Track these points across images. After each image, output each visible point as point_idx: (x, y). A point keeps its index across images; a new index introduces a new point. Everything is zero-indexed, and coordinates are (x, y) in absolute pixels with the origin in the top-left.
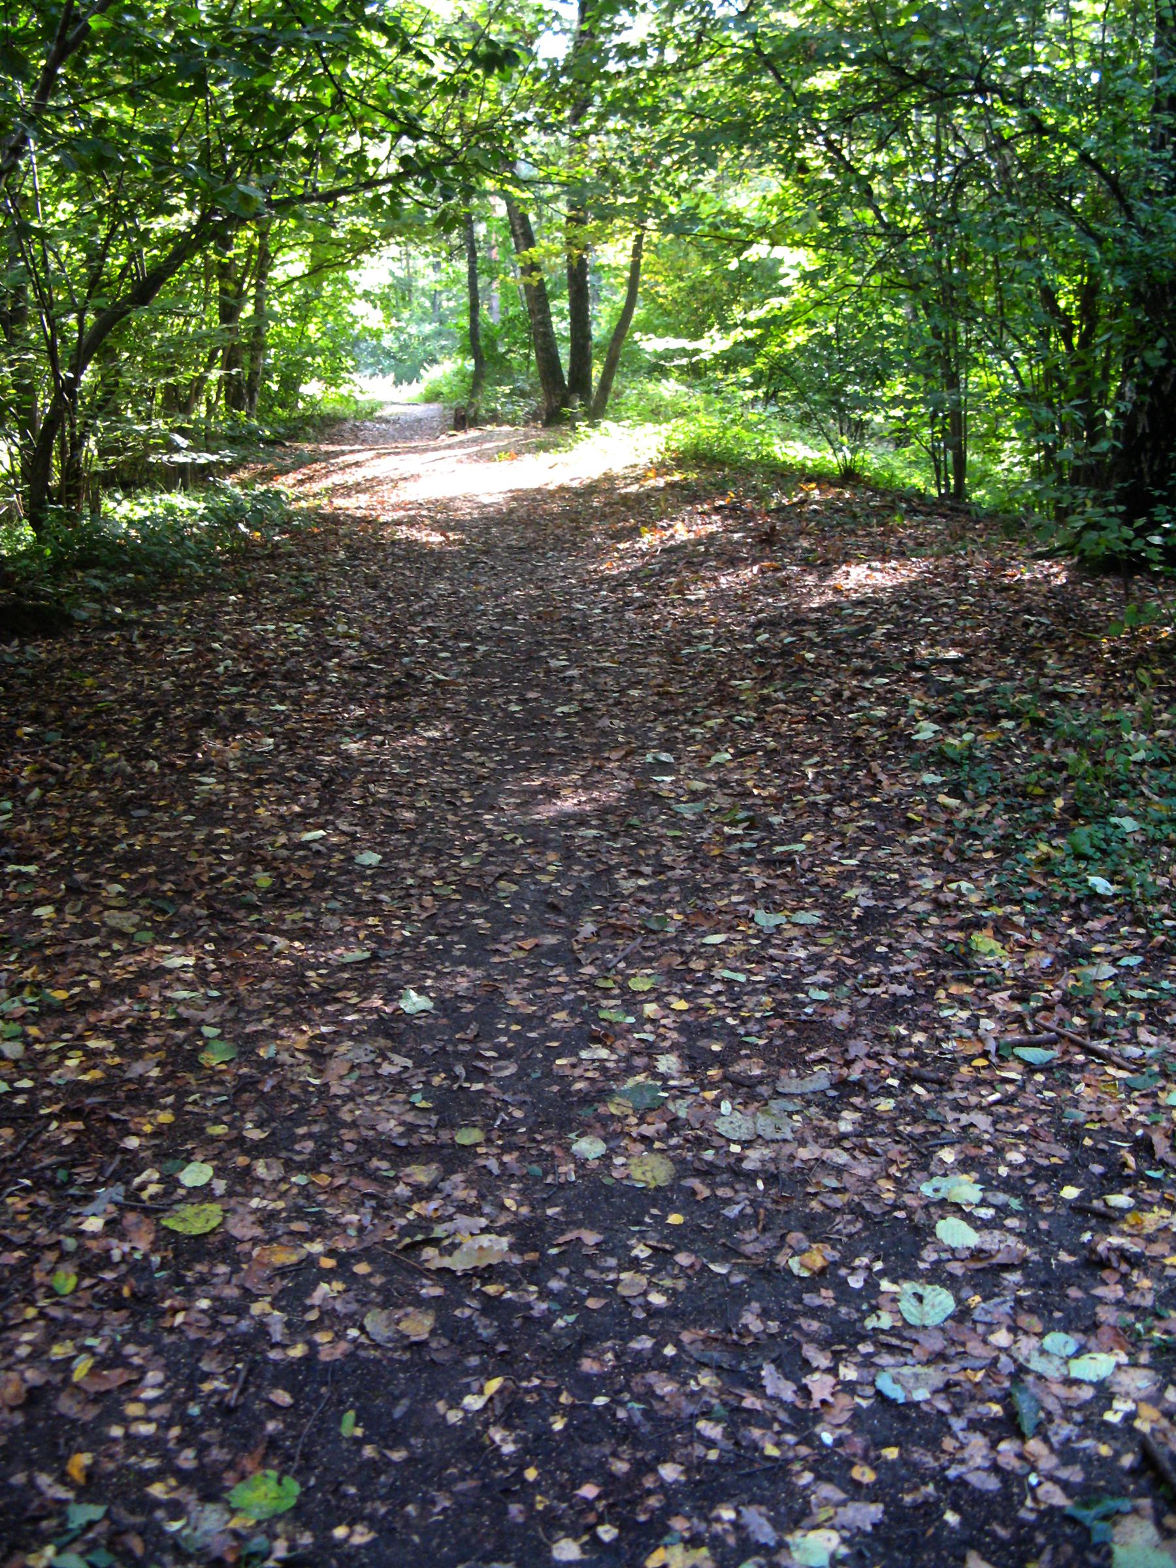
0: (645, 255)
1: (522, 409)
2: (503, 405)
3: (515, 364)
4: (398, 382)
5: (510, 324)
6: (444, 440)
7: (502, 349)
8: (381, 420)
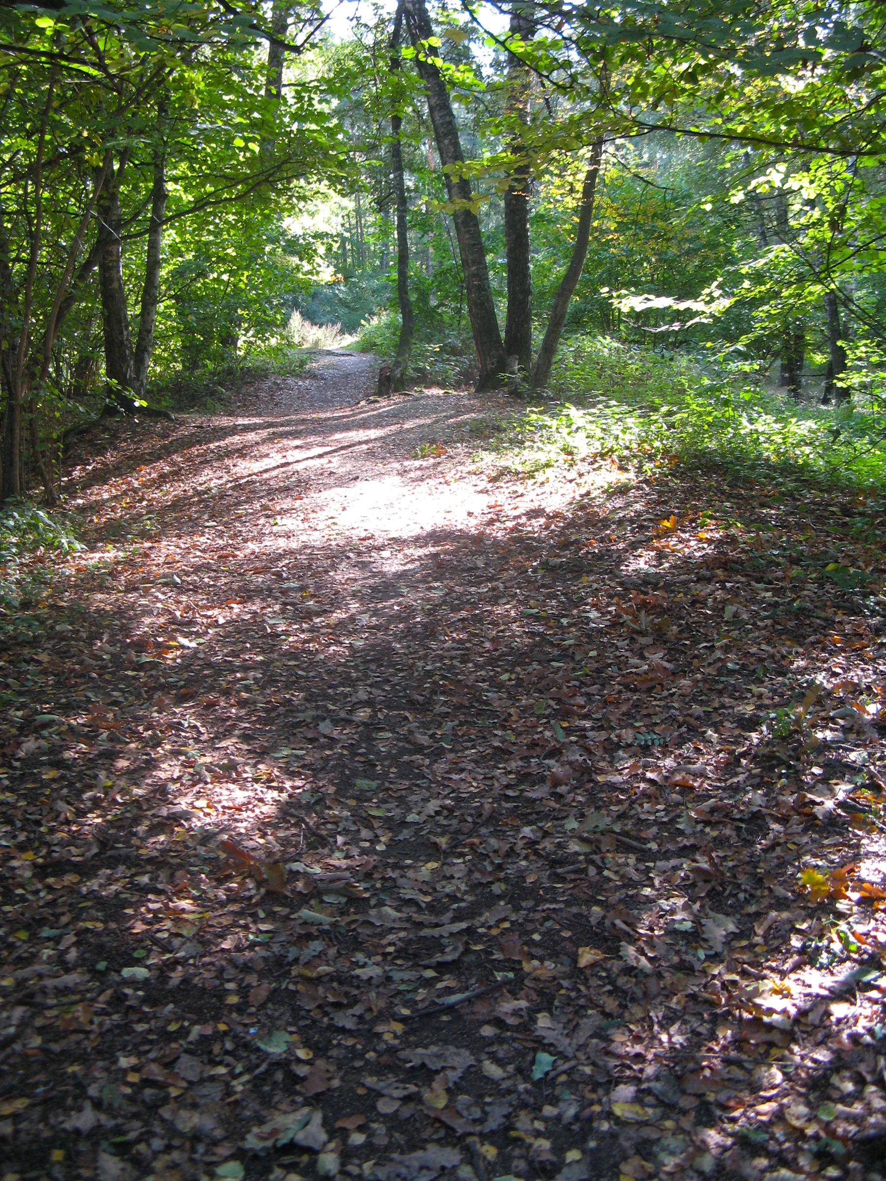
0: (597, 196)
1: (453, 370)
2: (432, 364)
3: (446, 318)
4: (342, 332)
5: (442, 275)
6: (365, 410)
7: (434, 303)
8: (313, 376)
